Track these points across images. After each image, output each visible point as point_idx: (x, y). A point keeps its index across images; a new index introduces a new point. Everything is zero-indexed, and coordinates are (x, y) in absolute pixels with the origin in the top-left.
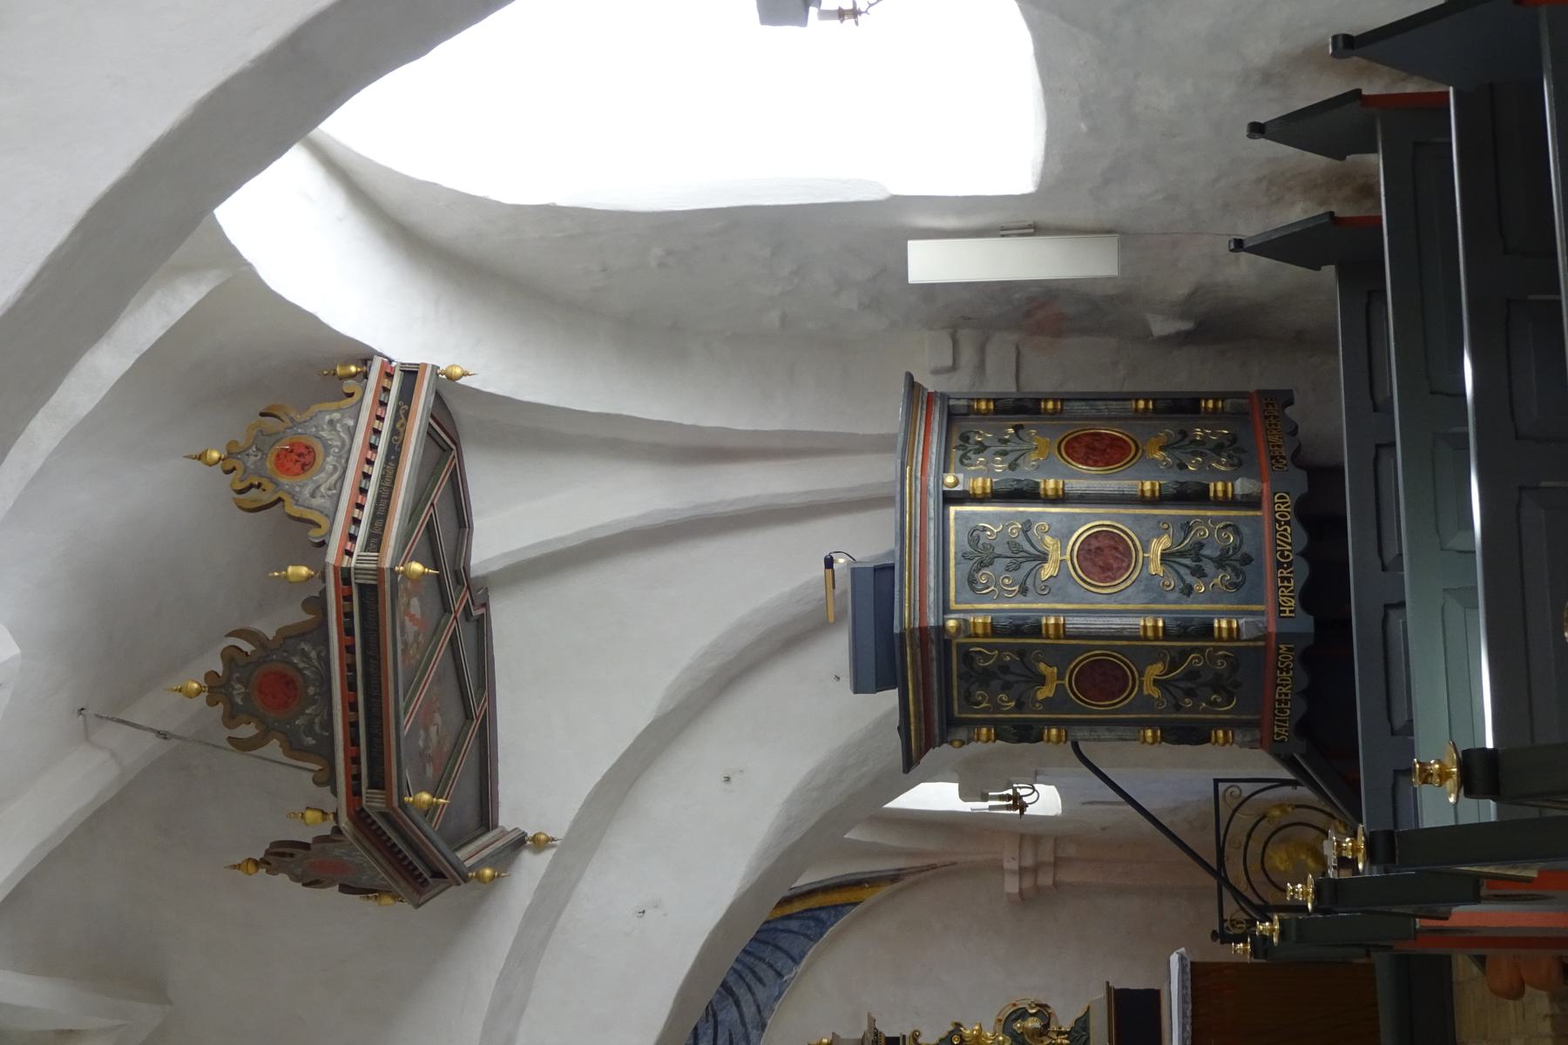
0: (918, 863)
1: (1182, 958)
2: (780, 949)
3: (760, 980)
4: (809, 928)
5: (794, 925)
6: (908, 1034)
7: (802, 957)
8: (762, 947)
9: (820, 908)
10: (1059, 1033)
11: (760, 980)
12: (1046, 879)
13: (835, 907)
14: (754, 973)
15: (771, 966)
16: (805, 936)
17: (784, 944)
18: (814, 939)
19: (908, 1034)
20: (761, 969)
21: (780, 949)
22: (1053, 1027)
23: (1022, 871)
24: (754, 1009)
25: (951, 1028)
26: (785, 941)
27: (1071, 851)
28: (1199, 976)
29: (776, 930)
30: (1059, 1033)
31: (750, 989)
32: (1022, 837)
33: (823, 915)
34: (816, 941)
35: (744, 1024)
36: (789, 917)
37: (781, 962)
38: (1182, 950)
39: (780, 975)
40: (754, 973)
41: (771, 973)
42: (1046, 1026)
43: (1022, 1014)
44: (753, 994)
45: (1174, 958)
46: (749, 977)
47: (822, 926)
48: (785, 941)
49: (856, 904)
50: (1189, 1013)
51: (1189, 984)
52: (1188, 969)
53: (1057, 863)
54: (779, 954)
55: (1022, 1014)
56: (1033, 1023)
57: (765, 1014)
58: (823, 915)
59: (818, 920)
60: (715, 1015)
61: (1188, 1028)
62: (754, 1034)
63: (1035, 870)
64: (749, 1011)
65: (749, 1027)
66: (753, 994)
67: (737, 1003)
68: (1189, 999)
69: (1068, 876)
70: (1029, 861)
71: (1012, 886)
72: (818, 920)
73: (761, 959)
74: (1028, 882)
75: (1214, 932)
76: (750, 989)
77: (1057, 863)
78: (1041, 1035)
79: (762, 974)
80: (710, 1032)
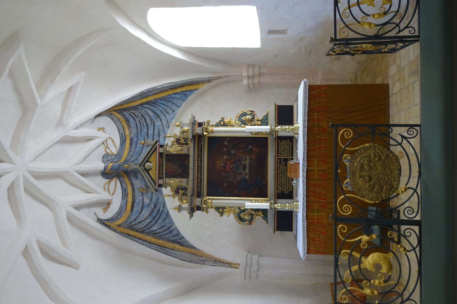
0: (216, 75)
1: (305, 83)
2: (174, 103)
3: (168, 113)
4: (183, 97)
5: (178, 96)
6: (206, 121)
7: (180, 106)
8: (168, 103)
9: (186, 91)
10: (258, 120)
11: (168, 113)
12: (256, 80)
13: (191, 90)
14: (166, 111)
15: (171, 109)
16: (182, 100)
17: (175, 102)
18: (184, 100)
19: (206, 121)
20: (168, 109)
21: (174, 103)
22: (256, 118)
23: (248, 77)
24: (166, 121)
25: (221, 119)
26: (175, 101)
27: (264, 70)
28: (313, 92)
29: (172, 97)
30: (258, 120)
31: (165, 116)
32: (249, 65)
33: (187, 93)
34: (184, 101)
35: (163, 126)
36: (176, 94)
37: (174, 107)
38: (305, 80)
39: (174, 111)
40: (166, 111)
41: (171, 111)
42: (253, 118)
43: (245, 114)
44: (166, 117)
45: (302, 83)
46: (164, 112)
47: (187, 96)
48: (175, 101)
49: (197, 89)
50: (307, 104)
51: (307, 93)
52: (307, 87)
53: (260, 75)
54: (174, 105)
55: (245, 114)
56: (248, 117)
57: (169, 123)
58: (187, 93)
59: (185, 94)
60: (154, 123)
61: (307, 109)
62: (166, 129)
63: (253, 77)
64: (164, 122)
65: (165, 127)
66: (166, 117)
67: (161, 120)
68: (307, 98)
69: (264, 80)
70: (251, 73)
71: (245, 82)
72: (185, 94)
73: (168, 107)
74: (251, 81)
75: (331, 38)
76: (165, 116)
77: (260, 75)
78: (251, 121)
79: (168, 111)
80: (152, 128)
